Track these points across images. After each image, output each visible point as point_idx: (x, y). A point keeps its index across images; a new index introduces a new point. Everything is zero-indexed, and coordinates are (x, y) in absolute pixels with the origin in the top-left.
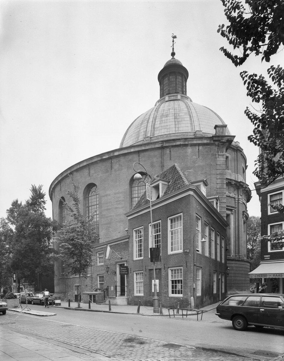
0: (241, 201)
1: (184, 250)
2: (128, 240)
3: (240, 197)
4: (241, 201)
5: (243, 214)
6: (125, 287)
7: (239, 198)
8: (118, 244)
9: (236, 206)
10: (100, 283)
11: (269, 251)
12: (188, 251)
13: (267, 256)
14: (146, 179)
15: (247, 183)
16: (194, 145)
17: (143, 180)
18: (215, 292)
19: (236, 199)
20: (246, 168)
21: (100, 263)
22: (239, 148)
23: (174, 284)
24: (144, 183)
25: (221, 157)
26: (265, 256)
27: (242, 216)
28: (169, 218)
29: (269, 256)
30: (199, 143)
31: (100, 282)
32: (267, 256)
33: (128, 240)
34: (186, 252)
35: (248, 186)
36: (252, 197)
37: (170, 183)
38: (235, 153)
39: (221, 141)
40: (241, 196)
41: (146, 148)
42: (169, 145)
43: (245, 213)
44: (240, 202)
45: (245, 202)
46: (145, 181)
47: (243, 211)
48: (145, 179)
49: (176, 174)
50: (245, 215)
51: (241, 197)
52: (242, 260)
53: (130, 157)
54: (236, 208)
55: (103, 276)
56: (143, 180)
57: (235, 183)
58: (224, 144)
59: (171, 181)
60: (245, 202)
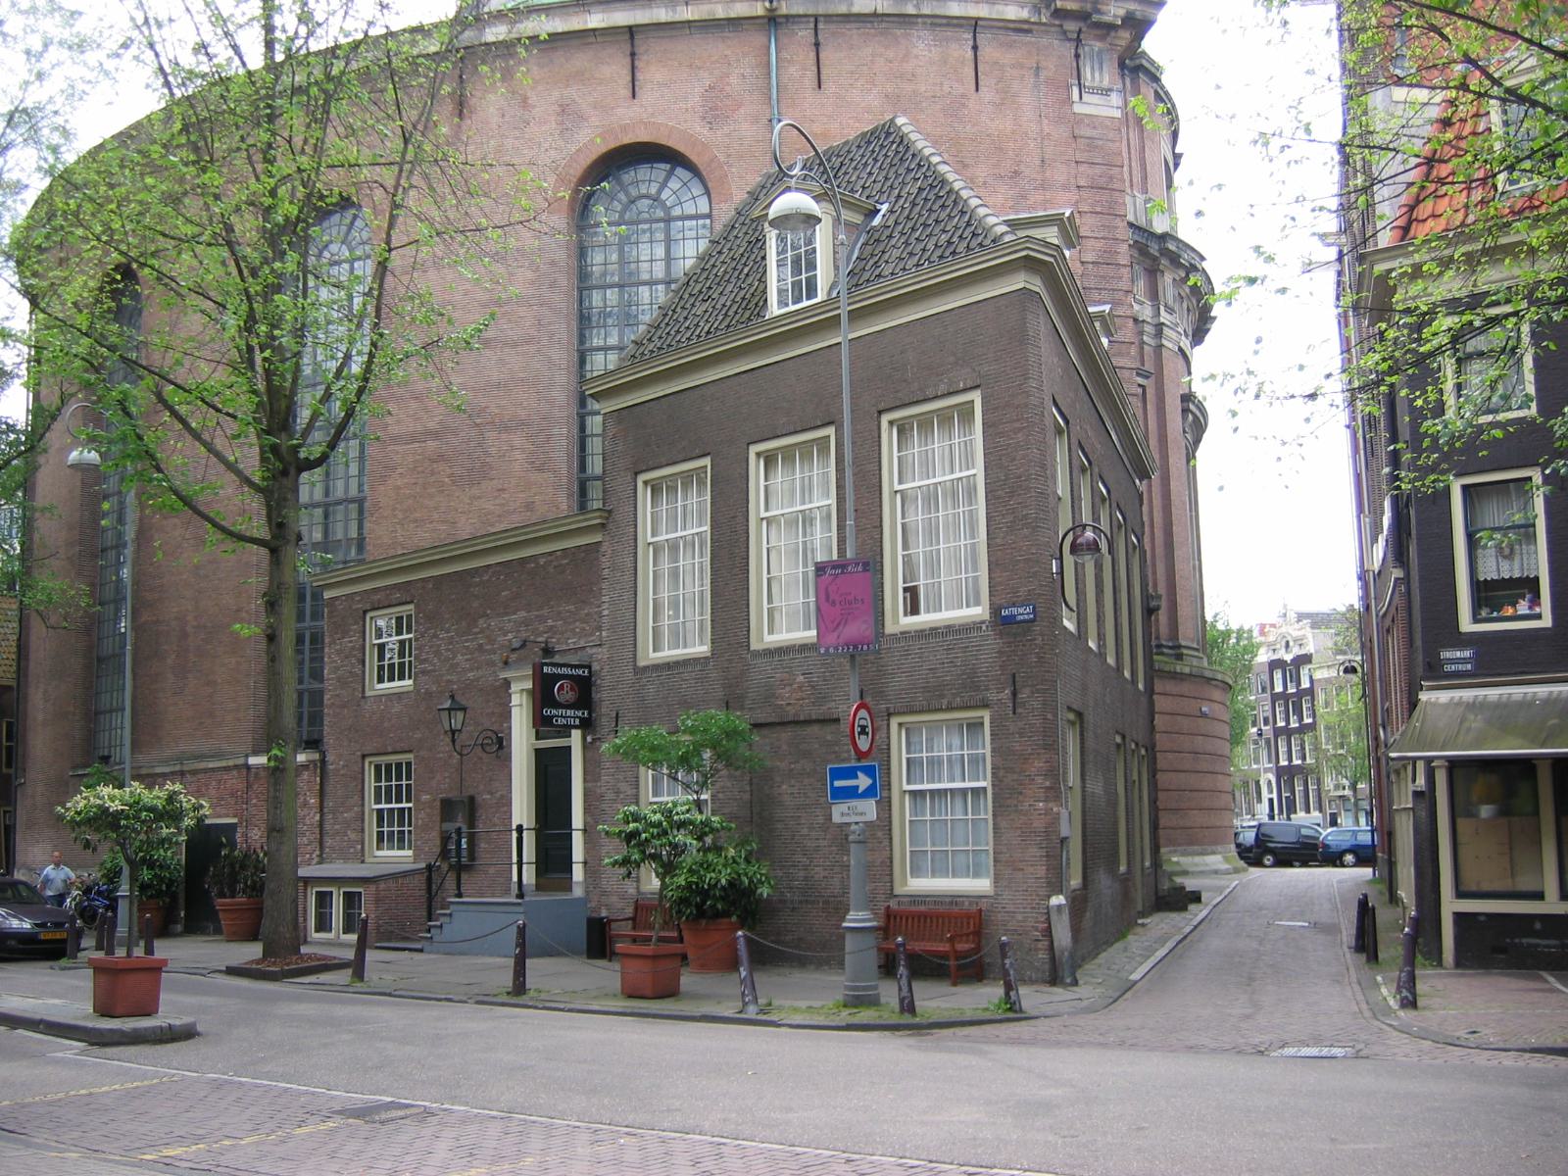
0: (1170, 340)
1: (995, 610)
2: (597, 538)
3: (1165, 318)
4: (1170, 340)
5: (1185, 411)
6: (570, 836)
7: (1162, 320)
8: (523, 561)
9: (1149, 366)
10: (380, 812)
11: (1467, 625)
12: (1023, 613)
13: (1458, 654)
14: (674, 184)
15: (1181, 235)
16: (948, 25)
17: (653, 191)
18: (1123, 868)
19: (1148, 328)
20: (1176, 165)
21: (381, 680)
22: (1144, 62)
23: (970, 816)
24: (663, 204)
25: (1095, 99)
26: (1446, 654)
27: (1179, 419)
28: (885, 419)
29: (1467, 654)
30: (977, 19)
31: (378, 801)
32: (1458, 654)
33: (597, 538)
34: (1009, 621)
35: (1203, 258)
36: (1215, 318)
37: (877, 221)
38: (1128, 81)
39: (1095, 18)
40: (1170, 310)
41: (677, 18)
42: (810, 12)
43: (1192, 407)
44: (1164, 342)
45: (1185, 343)
46: (663, 196)
47: (1182, 396)
48: (664, 185)
49: (909, 170)
50: (1190, 417)
51: (1168, 316)
52: (1194, 672)
53: (580, 60)
54: (1147, 377)
55: (409, 764)
56: (653, 191)
57: (1136, 238)
58: (1108, 34)
59: (884, 208)
60: (1185, 343)
